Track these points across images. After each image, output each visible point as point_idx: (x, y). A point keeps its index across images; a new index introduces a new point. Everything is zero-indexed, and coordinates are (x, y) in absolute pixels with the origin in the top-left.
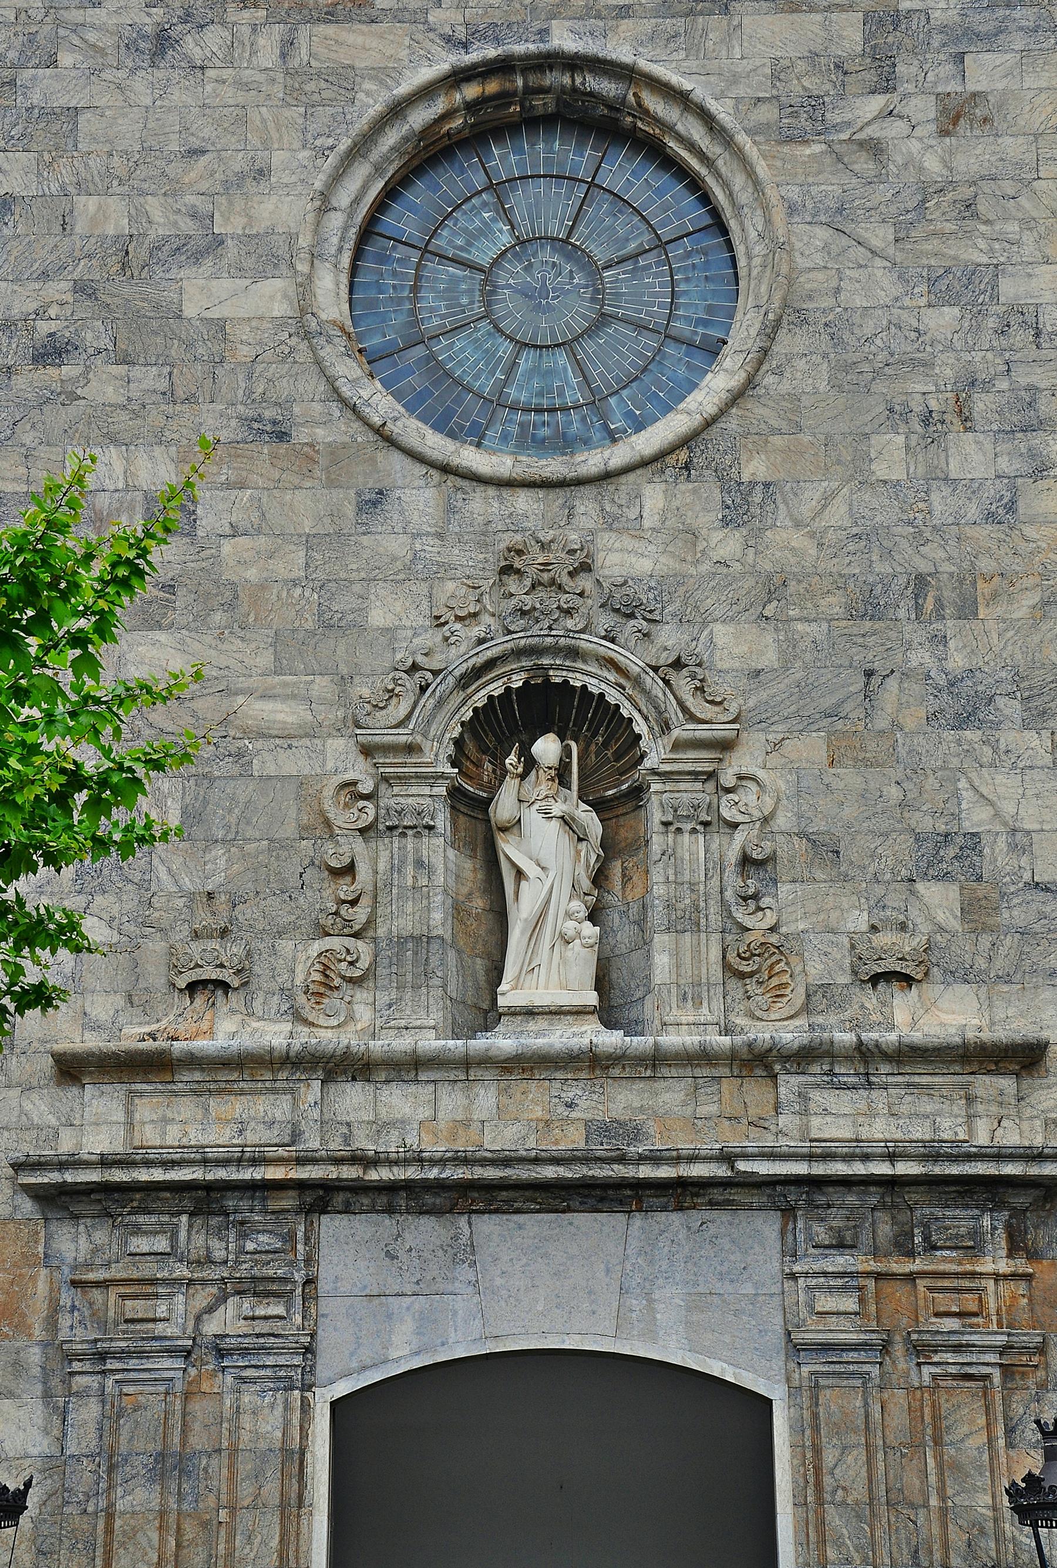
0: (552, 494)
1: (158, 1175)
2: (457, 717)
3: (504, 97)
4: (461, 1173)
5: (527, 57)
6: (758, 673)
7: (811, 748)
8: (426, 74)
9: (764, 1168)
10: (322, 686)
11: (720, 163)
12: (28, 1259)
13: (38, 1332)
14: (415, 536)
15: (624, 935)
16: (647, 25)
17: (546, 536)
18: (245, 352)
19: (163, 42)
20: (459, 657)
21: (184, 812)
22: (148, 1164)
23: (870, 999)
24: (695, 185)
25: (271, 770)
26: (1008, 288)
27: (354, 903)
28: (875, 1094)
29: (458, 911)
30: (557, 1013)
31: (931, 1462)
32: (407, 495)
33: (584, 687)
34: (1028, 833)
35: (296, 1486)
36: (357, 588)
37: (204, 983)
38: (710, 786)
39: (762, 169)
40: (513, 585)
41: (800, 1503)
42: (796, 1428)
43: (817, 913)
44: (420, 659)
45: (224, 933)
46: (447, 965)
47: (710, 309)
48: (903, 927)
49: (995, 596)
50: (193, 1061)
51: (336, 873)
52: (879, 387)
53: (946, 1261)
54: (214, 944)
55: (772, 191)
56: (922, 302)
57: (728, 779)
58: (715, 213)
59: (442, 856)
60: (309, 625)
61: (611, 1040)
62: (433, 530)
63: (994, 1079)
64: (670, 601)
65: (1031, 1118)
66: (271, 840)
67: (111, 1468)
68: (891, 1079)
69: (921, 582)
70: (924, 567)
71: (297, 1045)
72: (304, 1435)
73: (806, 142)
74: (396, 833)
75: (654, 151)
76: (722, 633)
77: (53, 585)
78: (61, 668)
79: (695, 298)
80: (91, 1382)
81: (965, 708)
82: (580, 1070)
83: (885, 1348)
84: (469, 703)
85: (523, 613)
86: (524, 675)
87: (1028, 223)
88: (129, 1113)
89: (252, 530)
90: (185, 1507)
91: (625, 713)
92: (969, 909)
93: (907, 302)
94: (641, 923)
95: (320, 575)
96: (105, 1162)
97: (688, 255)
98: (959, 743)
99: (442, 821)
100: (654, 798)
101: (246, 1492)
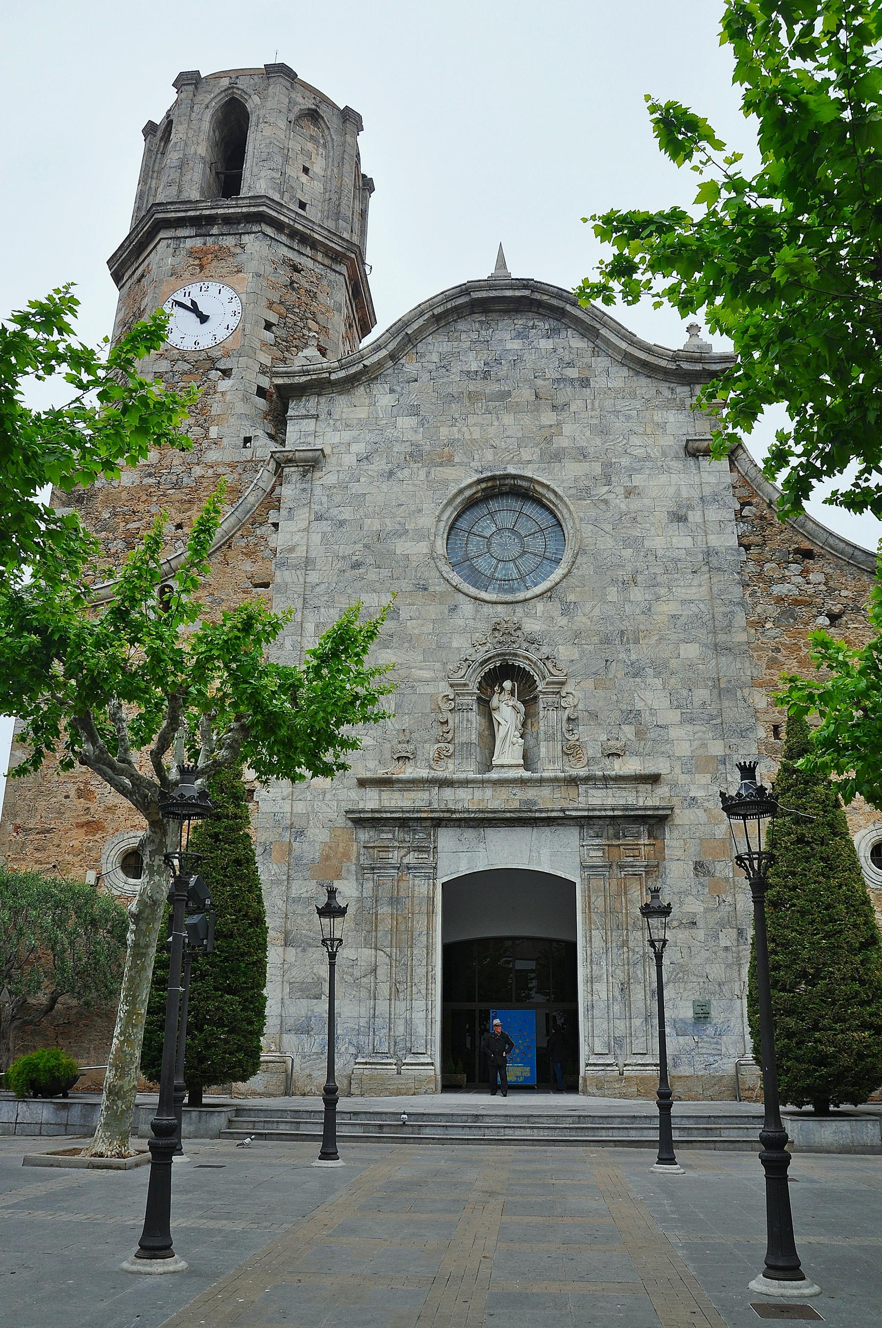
1: (389, 815)
3: (493, 487)
4: (481, 815)
5: (500, 475)
7: (589, 684)
8: (470, 481)
9: (574, 813)
12: (351, 840)
13: (354, 861)
16: (537, 466)
18: (415, 564)
19: (391, 473)
20: (480, 657)
22: (386, 812)
23: (607, 761)
24: (552, 512)
27: (448, 733)
29: (480, 735)
36: (448, 635)
38: (558, 696)
42: (583, 891)
45: (408, 741)
46: (477, 752)
47: (556, 549)
48: (617, 739)
50: (399, 781)
51: (442, 723)
53: (629, 840)
54: (405, 745)
55: (576, 515)
58: (558, 520)
59: (475, 718)
61: (527, 774)
69: (622, 632)
70: (624, 628)
71: (430, 776)
72: (434, 893)
75: (539, 502)
77: (350, 639)
78: (351, 664)
79: (552, 547)
80: (370, 876)
81: (636, 672)
83: (610, 867)
87: (652, 524)
88: (380, 796)
89: (418, 616)
94: (537, 738)
96: (373, 811)
97: (550, 533)
99: (475, 707)
101: (417, 908)
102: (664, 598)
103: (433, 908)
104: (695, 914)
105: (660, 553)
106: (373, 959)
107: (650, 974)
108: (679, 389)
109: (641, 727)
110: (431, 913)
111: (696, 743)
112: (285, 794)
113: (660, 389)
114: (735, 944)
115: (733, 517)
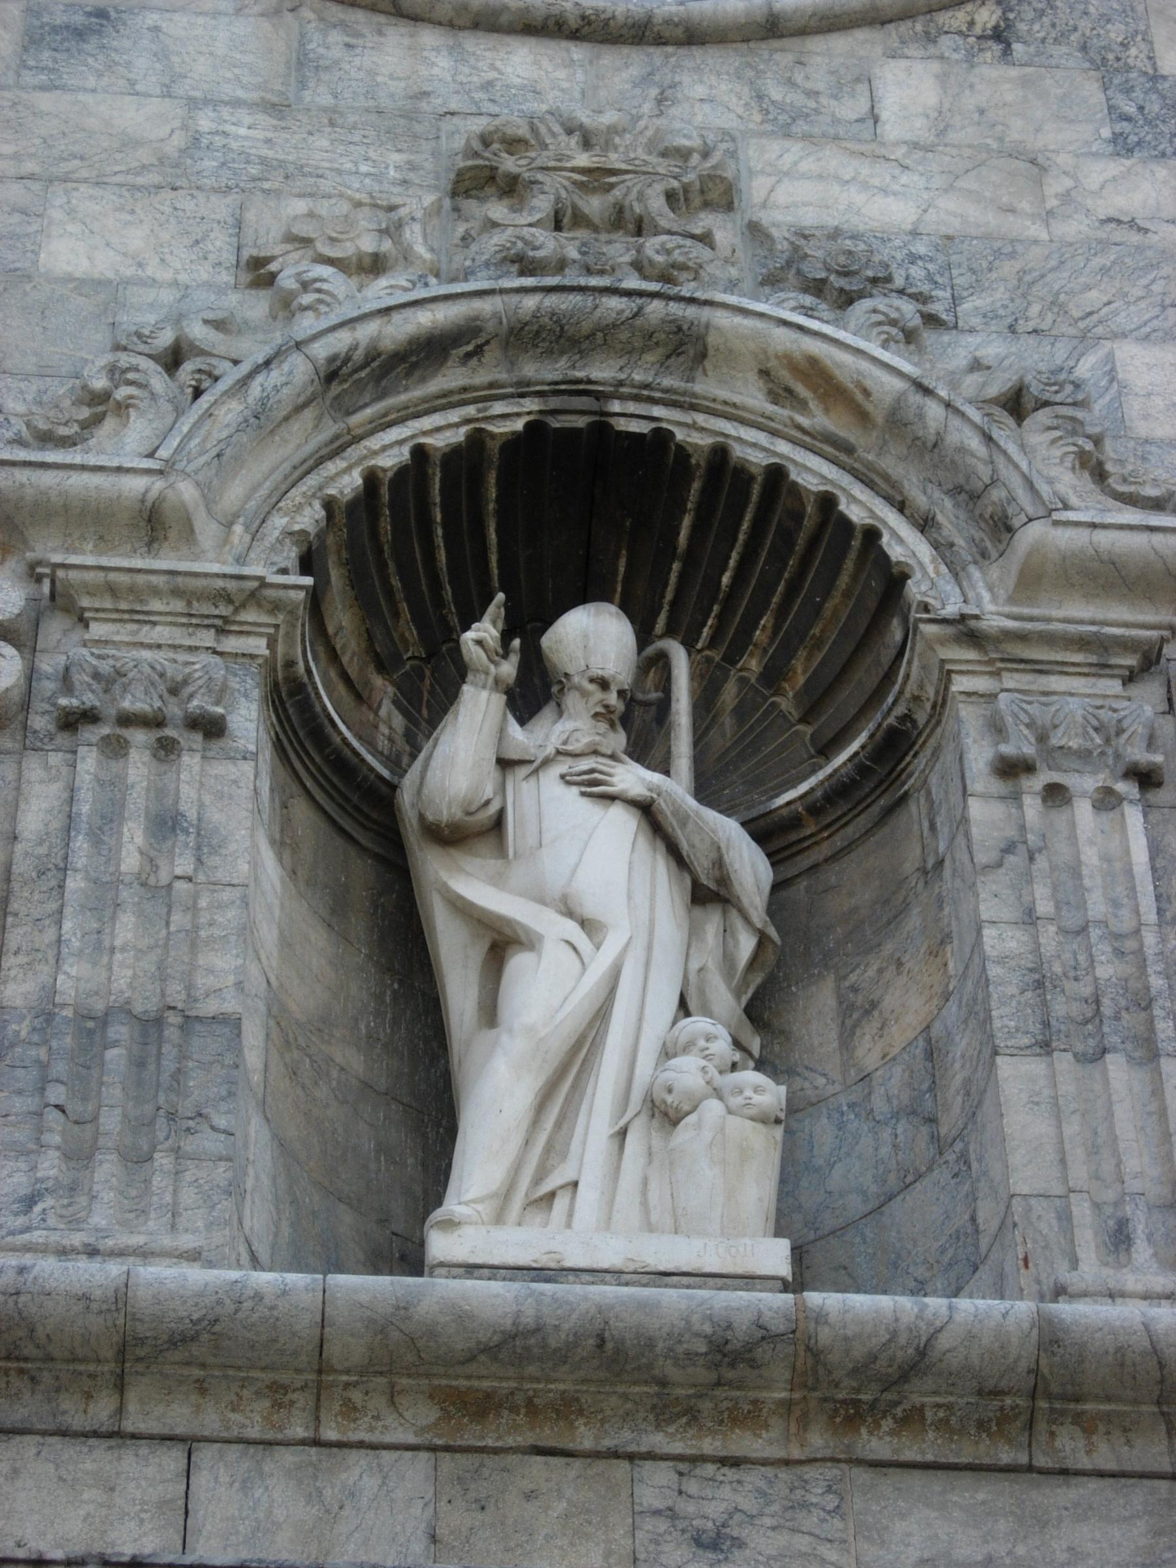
0: (610, 57)
2: (312, 481)
14: (193, 104)
33: (720, 453)
44: (197, 331)
62: (254, 96)
64: (976, 287)
74: (93, 733)
82: (747, 1417)
84: (354, 452)
86: (532, 405)
99: (248, 720)
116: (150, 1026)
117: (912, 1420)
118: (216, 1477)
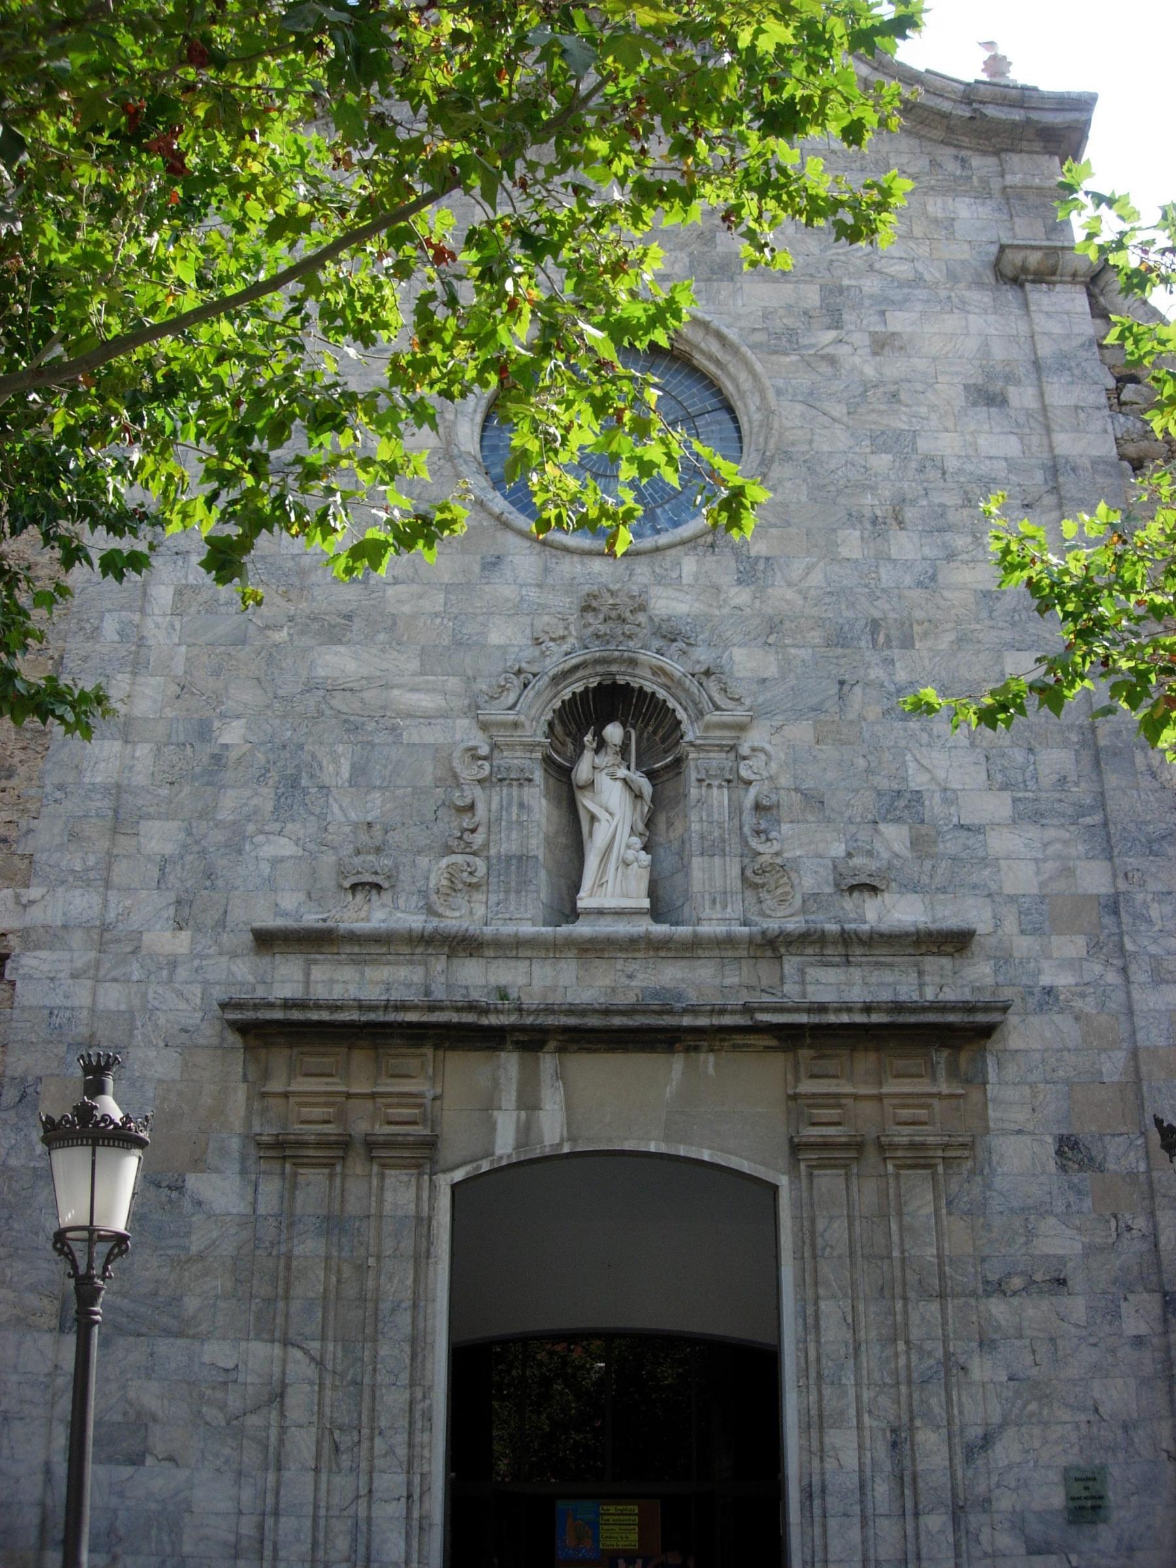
6: (764, 680)
10: (453, 683)
11: (730, 366)
14: (521, 586)
15: (668, 862)
17: (615, 587)
20: (555, 663)
21: (353, 767)
25: (416, 739)
26: (923, 445)
27: (473, 831)
28: (852, 970)
29: (549, 842)
30: (619, 913)
31: (894, 1227)
32: (517, 559)
34: (955, 791)
35: (425, 1243)
36: (480, 619)
37: (363, 884)
38: (732, 755)
39: (758, 367)
40: (590, 617)
41: (799, 1257)
42: (797, 1204)
43: (810, 843)
44: (524, 665)
45: (378, 850)
49: (926, 634)
50: (354, 938)
52: (842, 500)
54: (372, 858)
56: (868, 450)
57: (745, 750)
60: (446, 643)
61: (661, 929)
63: (937, 959)
64: (702, 632)
65: (962, 986)
66: (415, 788)
67: (291, 1225)
68: (864, 959)
70: (877, 614)
71: (430, 927)
72: (432, 1208)
73: (786, 354)
76: (739, 654)
82: (639, 950)
85: (598, 637)
86: (598, 679)
87: (933, 408)
88: (307, 975)
90: (343, 1254)
91: (670, 705)
92: (916, 843)
93: (857, 449)
94: (680, 854)
95: (455, 610)
96: (287, 1004)
98: (905, 730)
99: (538, 775)
100: (692, 764)
101: (388, 1246)
102: (965, 557)
103: (430, 1243)
104: (1062, 1259)
105: (952, 464)
106: (277, 1369)
107: (960, 1405)
108: (976, 161)
109: (924, 829)
110: (421, 1258)
111: (1050, 866)
112: (79, 964)
113: (939, 159)
114: (1159, 1328)
115: (1103, 400)
116: (520, 858)
117: (669, 949)
118: (536, 967)
